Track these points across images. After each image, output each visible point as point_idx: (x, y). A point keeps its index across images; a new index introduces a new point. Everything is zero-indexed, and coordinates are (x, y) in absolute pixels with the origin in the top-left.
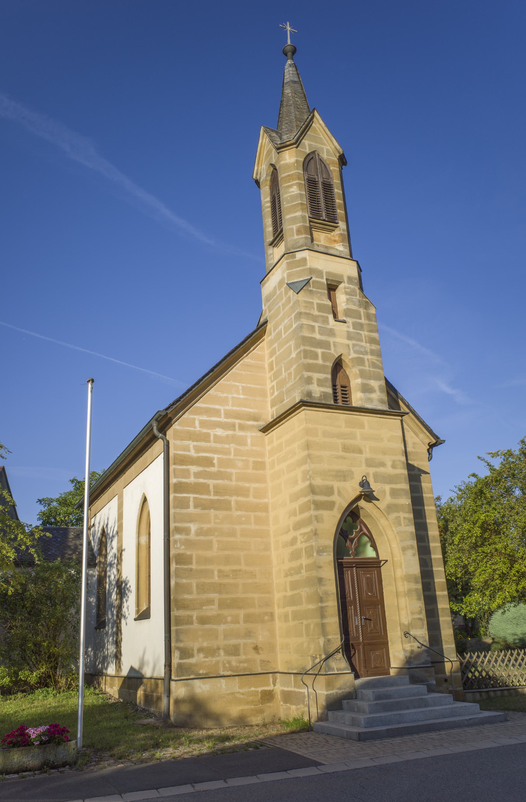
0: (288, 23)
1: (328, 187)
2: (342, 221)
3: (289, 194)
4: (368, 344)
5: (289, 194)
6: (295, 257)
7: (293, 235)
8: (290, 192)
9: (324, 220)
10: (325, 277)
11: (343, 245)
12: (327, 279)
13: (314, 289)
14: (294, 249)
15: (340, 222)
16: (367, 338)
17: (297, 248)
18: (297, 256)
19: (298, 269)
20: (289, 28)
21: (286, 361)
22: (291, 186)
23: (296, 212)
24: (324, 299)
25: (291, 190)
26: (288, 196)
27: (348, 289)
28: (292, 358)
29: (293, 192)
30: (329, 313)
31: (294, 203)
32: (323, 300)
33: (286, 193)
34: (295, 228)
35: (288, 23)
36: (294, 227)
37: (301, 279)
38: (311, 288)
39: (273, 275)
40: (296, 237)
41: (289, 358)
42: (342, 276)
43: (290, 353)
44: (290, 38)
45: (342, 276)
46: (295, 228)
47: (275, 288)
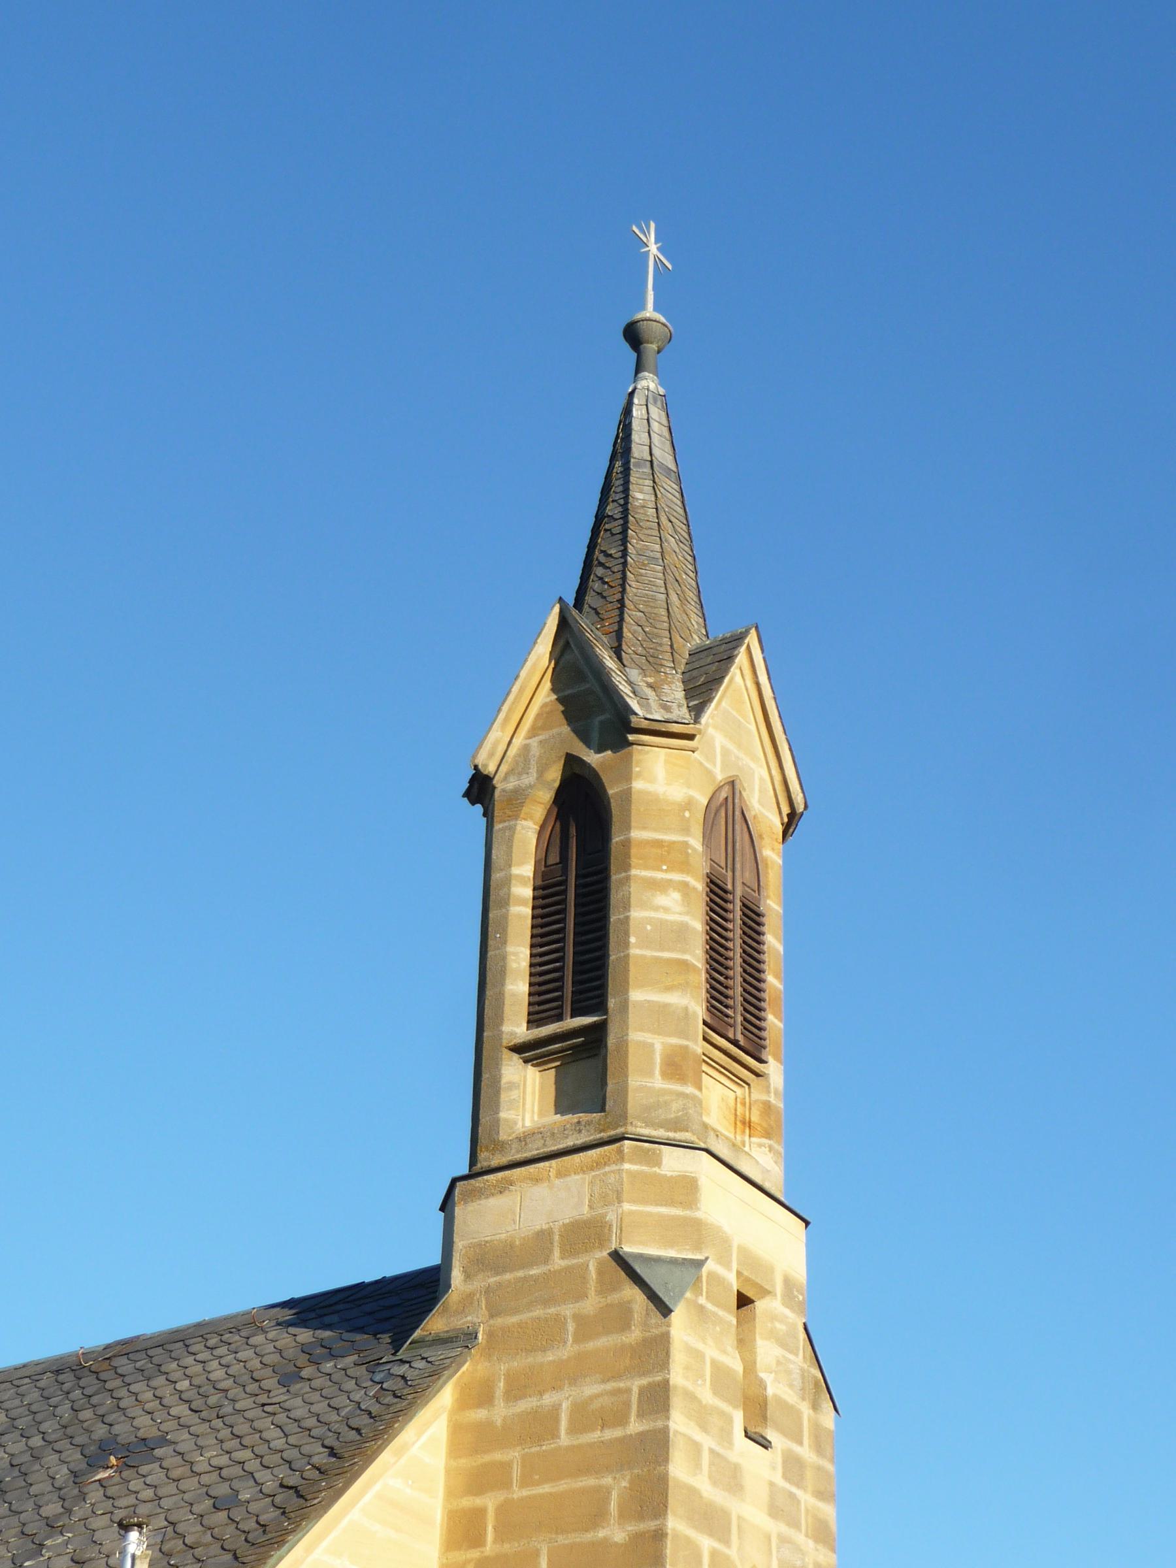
0: (653, 225)
1: (753, 919)
2: (777, 1059)
3: (653, 914)
4: (811, 1543)
5: (653, 914)
6: (658, 1164)
7: (651, 1074)
8: (657, 909)
9: (735, 1043)
10: (735, 1266)
11: (771, 1148)
12: (739, 1273)
13: (709, 1306)
14: (649, 1124)
15: (771, 1059)
16: (810, 1520)
17: (661, 1125)
18: (665, 1161)
19: (663, 1210)
20: (653, 249)
21: (562, 1540)
22: (661, 886)
23: (668, 989)
24: (729, 1349)
25: (661, 900)
26: (650, 920)
27: (781, 1321)
28: (605, 1543)
29: (666, 910)
30: (736, 1407)
31: (666, 955)
32: (725, 1352)
33: (643, 905)
34: (658, 1048)
35: (653, 225)
36: (659, 1044)
37: (672, 1253)
38: (702, 1300)
39: (537, 1180)
40: (658, 1082)
41: (589, 1536)
42: (771, 1270)
43: (598, 1517)
44: (654, 289)
45: (769, 1270)
46: (658, 1048)
47: (543, 1237)
